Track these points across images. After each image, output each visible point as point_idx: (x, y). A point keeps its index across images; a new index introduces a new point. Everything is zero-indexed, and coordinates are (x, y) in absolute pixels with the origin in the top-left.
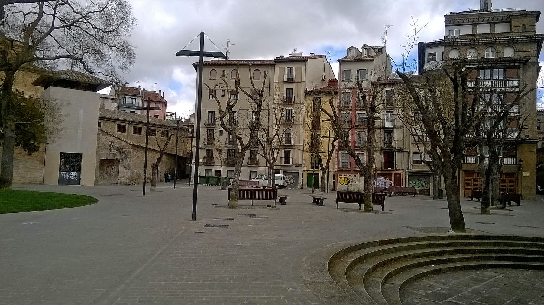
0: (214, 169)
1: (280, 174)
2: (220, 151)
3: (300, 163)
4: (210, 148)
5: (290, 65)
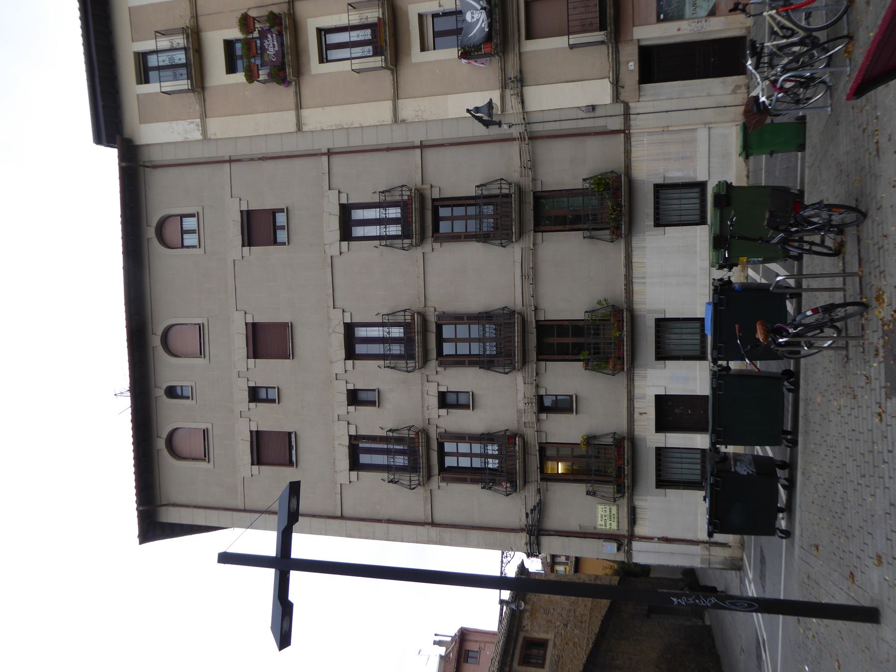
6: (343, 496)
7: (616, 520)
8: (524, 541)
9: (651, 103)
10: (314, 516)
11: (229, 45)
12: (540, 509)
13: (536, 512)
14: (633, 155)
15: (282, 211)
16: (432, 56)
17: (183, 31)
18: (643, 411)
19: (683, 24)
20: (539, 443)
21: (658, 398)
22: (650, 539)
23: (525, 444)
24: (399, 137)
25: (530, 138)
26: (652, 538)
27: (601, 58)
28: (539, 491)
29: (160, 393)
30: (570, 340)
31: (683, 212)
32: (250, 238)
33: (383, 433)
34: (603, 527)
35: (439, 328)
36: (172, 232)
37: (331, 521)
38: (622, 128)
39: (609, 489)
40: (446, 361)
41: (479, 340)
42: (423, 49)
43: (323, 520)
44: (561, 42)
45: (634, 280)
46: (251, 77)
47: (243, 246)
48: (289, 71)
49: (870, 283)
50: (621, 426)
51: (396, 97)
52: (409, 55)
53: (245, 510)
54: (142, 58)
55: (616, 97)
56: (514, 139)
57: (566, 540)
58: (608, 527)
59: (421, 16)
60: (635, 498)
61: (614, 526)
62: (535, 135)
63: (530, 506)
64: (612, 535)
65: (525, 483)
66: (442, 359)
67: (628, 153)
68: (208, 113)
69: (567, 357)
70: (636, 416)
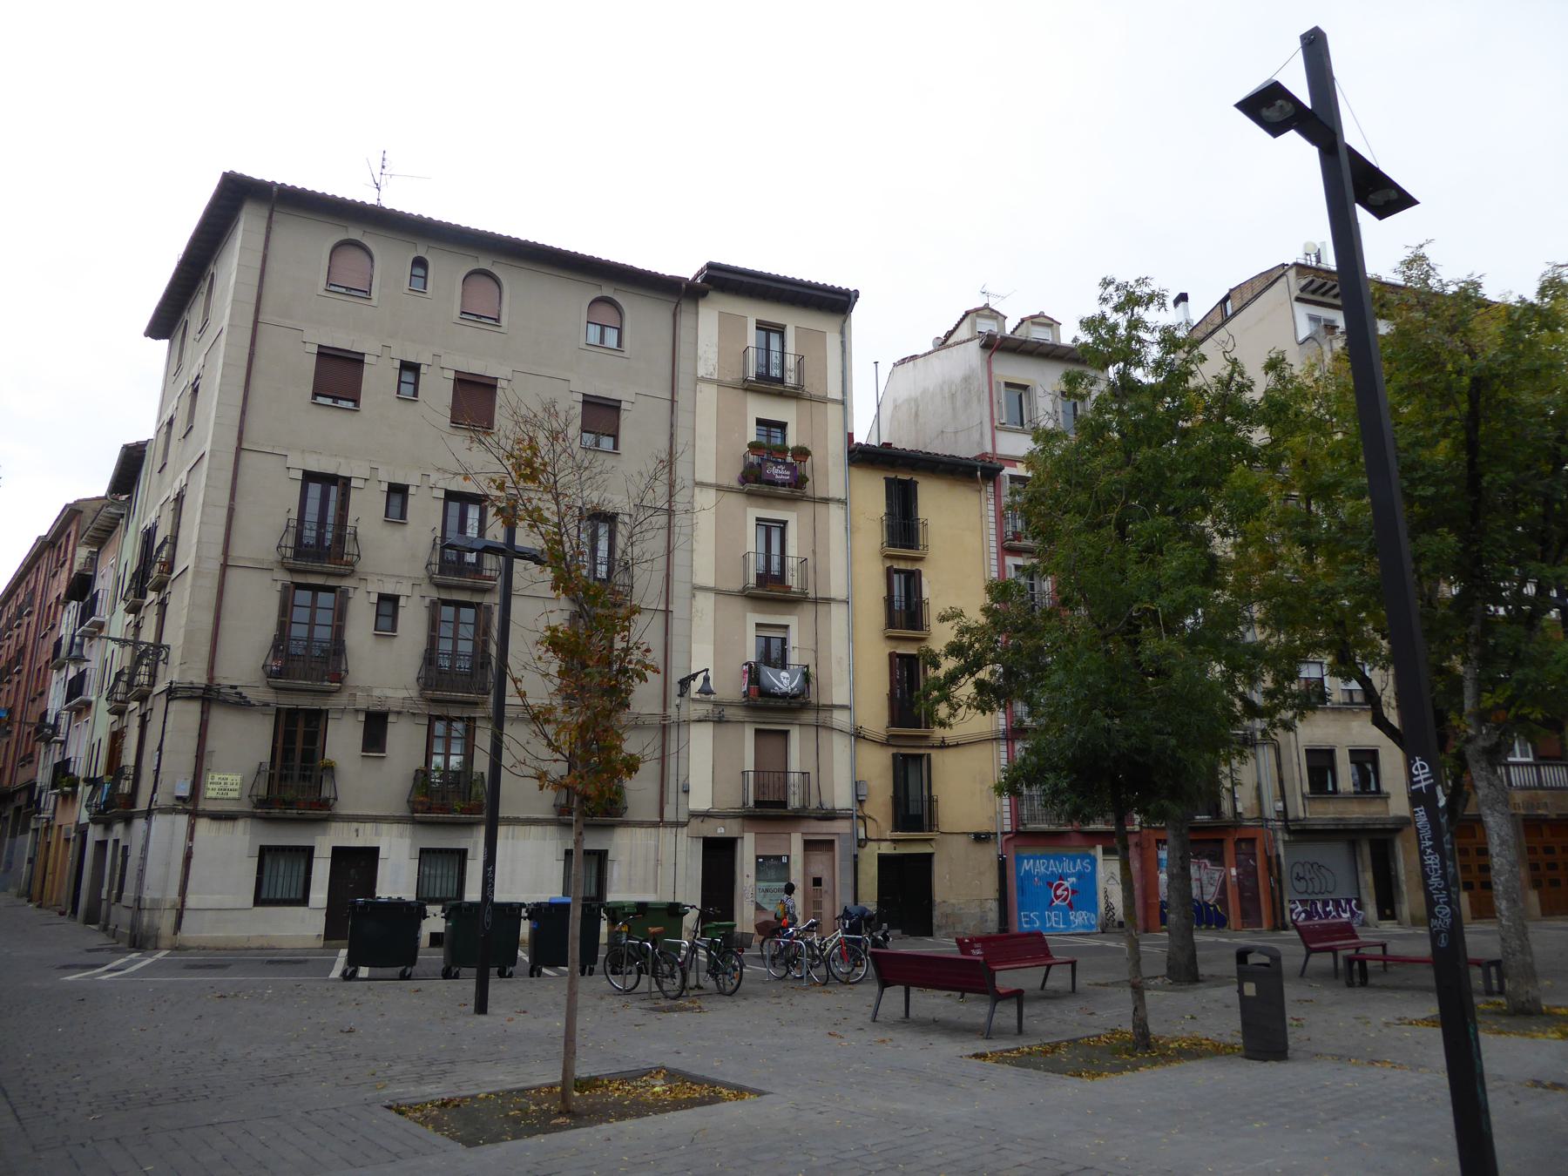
0: (325, 842)
1: (921, 830)
2: (388, 604)
3: (842, 798)
4: (306, 702)
5: (773, 314)
6: (270, 456)
7: (219, 796)
8: (195, 681)
9: (685, 848)
10: (243, 412)
11: (782, 426)
12: (240, 703)
13: (237, 700)
14: (638, 829)
15: (616, 446)
16: (751, 633)
17: (800, 386)
18: (360, 832)
19: (752, 880)
20: (327, 710)
21: (374, 851)
22: (191, 836)
23: (329, 693)
24: (679, 589)
25: (664, 726)
26: (191, 839)
27: (732, 801)
28: (267, 705)
29: (421, 251)
30: (299, 745)
31: (432, 880)
32: (326, 355)
33: (351, 522)
34: (210, 781)
35: (331, 589)
36: (605, 313)
37: (235, 434)
38: (665, 820)
39: (262, 790)
40: (435, 607)
41: (310, 638)
42: (758, 625)
43: (237, 422)
44: (749, 765)
45: (511, 827)
46: (754, 447)
47: (320, 346)
48: (754, 486)
49: (1523, 1003)
50: (343, 808)
51: (718, 592)
52: (755, 611)
53: (256, 322)
54: (780, 330)
55: (695, 815)
56: (665, 710)
57: (195, 733)
58: (210, 786)
59: (786, 627)
60: (249, 821)
61: (210, 794)
62: (667, 730)
63: (245, 692)
64: (199, 791)
65: (277, 689)
66: (292, 589)
67: (641, 824)
68: (721, 388)
69: (280, 741)
70: (355, 825)
